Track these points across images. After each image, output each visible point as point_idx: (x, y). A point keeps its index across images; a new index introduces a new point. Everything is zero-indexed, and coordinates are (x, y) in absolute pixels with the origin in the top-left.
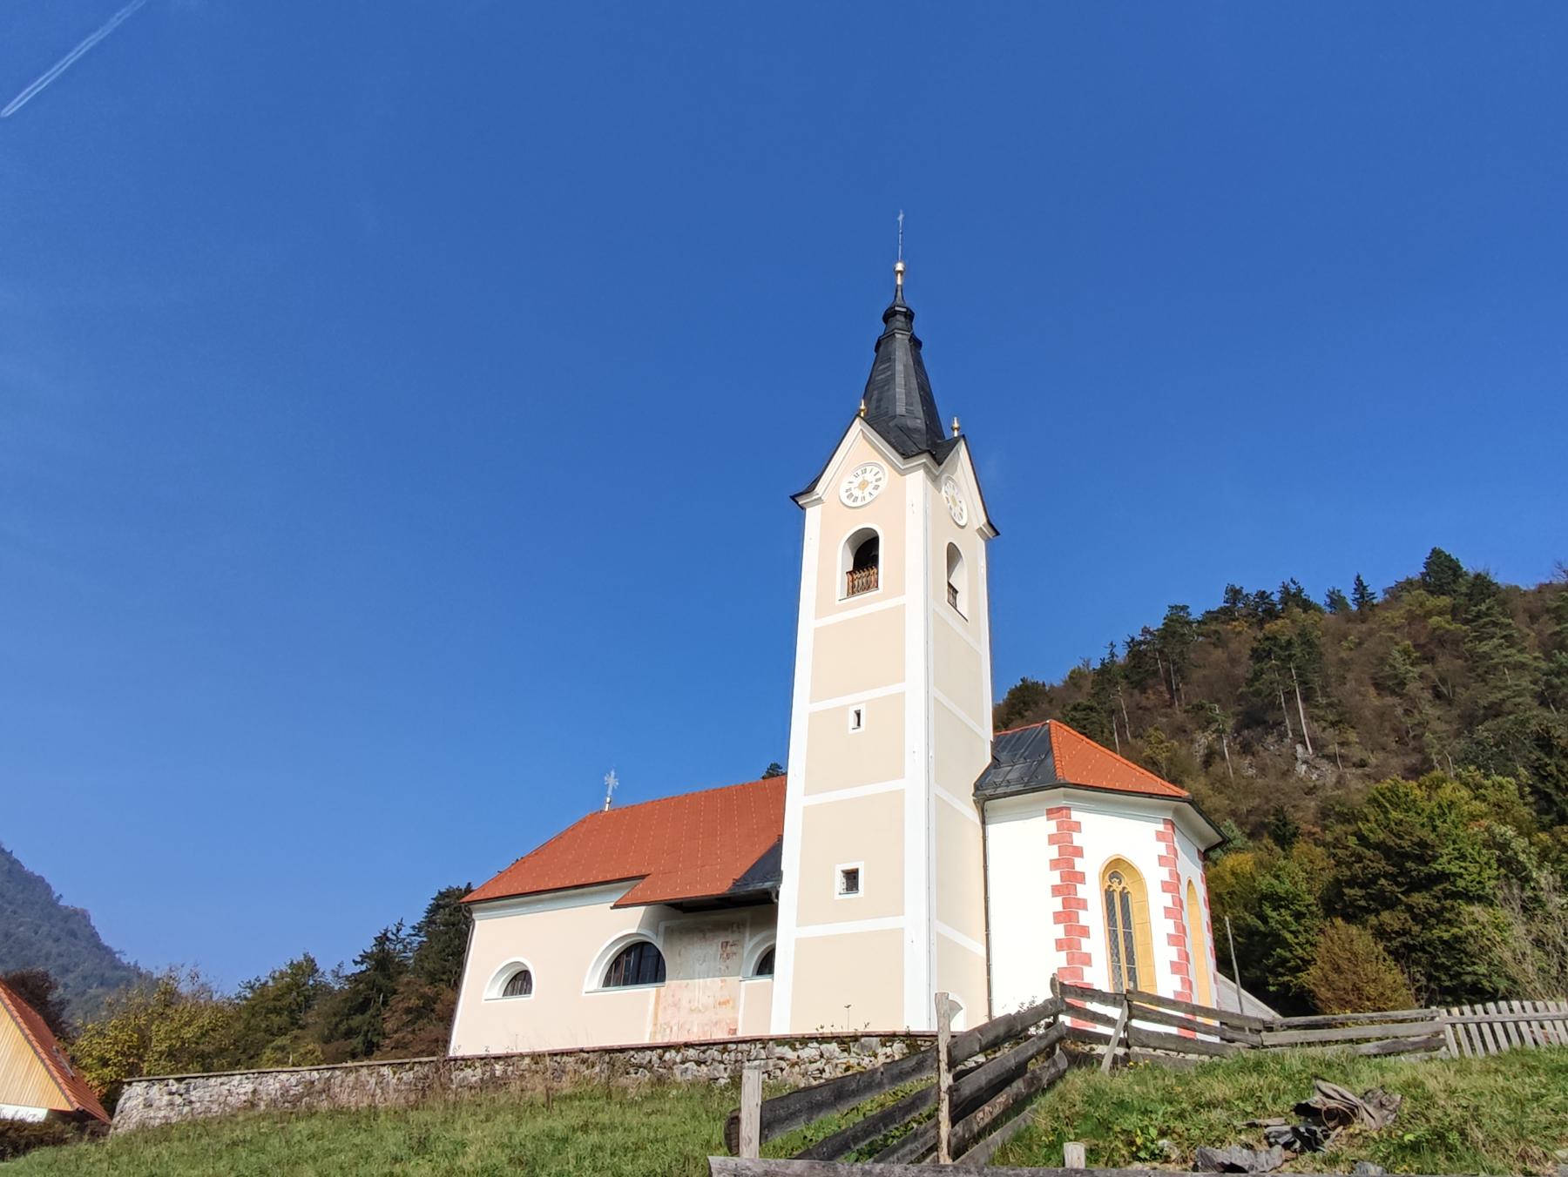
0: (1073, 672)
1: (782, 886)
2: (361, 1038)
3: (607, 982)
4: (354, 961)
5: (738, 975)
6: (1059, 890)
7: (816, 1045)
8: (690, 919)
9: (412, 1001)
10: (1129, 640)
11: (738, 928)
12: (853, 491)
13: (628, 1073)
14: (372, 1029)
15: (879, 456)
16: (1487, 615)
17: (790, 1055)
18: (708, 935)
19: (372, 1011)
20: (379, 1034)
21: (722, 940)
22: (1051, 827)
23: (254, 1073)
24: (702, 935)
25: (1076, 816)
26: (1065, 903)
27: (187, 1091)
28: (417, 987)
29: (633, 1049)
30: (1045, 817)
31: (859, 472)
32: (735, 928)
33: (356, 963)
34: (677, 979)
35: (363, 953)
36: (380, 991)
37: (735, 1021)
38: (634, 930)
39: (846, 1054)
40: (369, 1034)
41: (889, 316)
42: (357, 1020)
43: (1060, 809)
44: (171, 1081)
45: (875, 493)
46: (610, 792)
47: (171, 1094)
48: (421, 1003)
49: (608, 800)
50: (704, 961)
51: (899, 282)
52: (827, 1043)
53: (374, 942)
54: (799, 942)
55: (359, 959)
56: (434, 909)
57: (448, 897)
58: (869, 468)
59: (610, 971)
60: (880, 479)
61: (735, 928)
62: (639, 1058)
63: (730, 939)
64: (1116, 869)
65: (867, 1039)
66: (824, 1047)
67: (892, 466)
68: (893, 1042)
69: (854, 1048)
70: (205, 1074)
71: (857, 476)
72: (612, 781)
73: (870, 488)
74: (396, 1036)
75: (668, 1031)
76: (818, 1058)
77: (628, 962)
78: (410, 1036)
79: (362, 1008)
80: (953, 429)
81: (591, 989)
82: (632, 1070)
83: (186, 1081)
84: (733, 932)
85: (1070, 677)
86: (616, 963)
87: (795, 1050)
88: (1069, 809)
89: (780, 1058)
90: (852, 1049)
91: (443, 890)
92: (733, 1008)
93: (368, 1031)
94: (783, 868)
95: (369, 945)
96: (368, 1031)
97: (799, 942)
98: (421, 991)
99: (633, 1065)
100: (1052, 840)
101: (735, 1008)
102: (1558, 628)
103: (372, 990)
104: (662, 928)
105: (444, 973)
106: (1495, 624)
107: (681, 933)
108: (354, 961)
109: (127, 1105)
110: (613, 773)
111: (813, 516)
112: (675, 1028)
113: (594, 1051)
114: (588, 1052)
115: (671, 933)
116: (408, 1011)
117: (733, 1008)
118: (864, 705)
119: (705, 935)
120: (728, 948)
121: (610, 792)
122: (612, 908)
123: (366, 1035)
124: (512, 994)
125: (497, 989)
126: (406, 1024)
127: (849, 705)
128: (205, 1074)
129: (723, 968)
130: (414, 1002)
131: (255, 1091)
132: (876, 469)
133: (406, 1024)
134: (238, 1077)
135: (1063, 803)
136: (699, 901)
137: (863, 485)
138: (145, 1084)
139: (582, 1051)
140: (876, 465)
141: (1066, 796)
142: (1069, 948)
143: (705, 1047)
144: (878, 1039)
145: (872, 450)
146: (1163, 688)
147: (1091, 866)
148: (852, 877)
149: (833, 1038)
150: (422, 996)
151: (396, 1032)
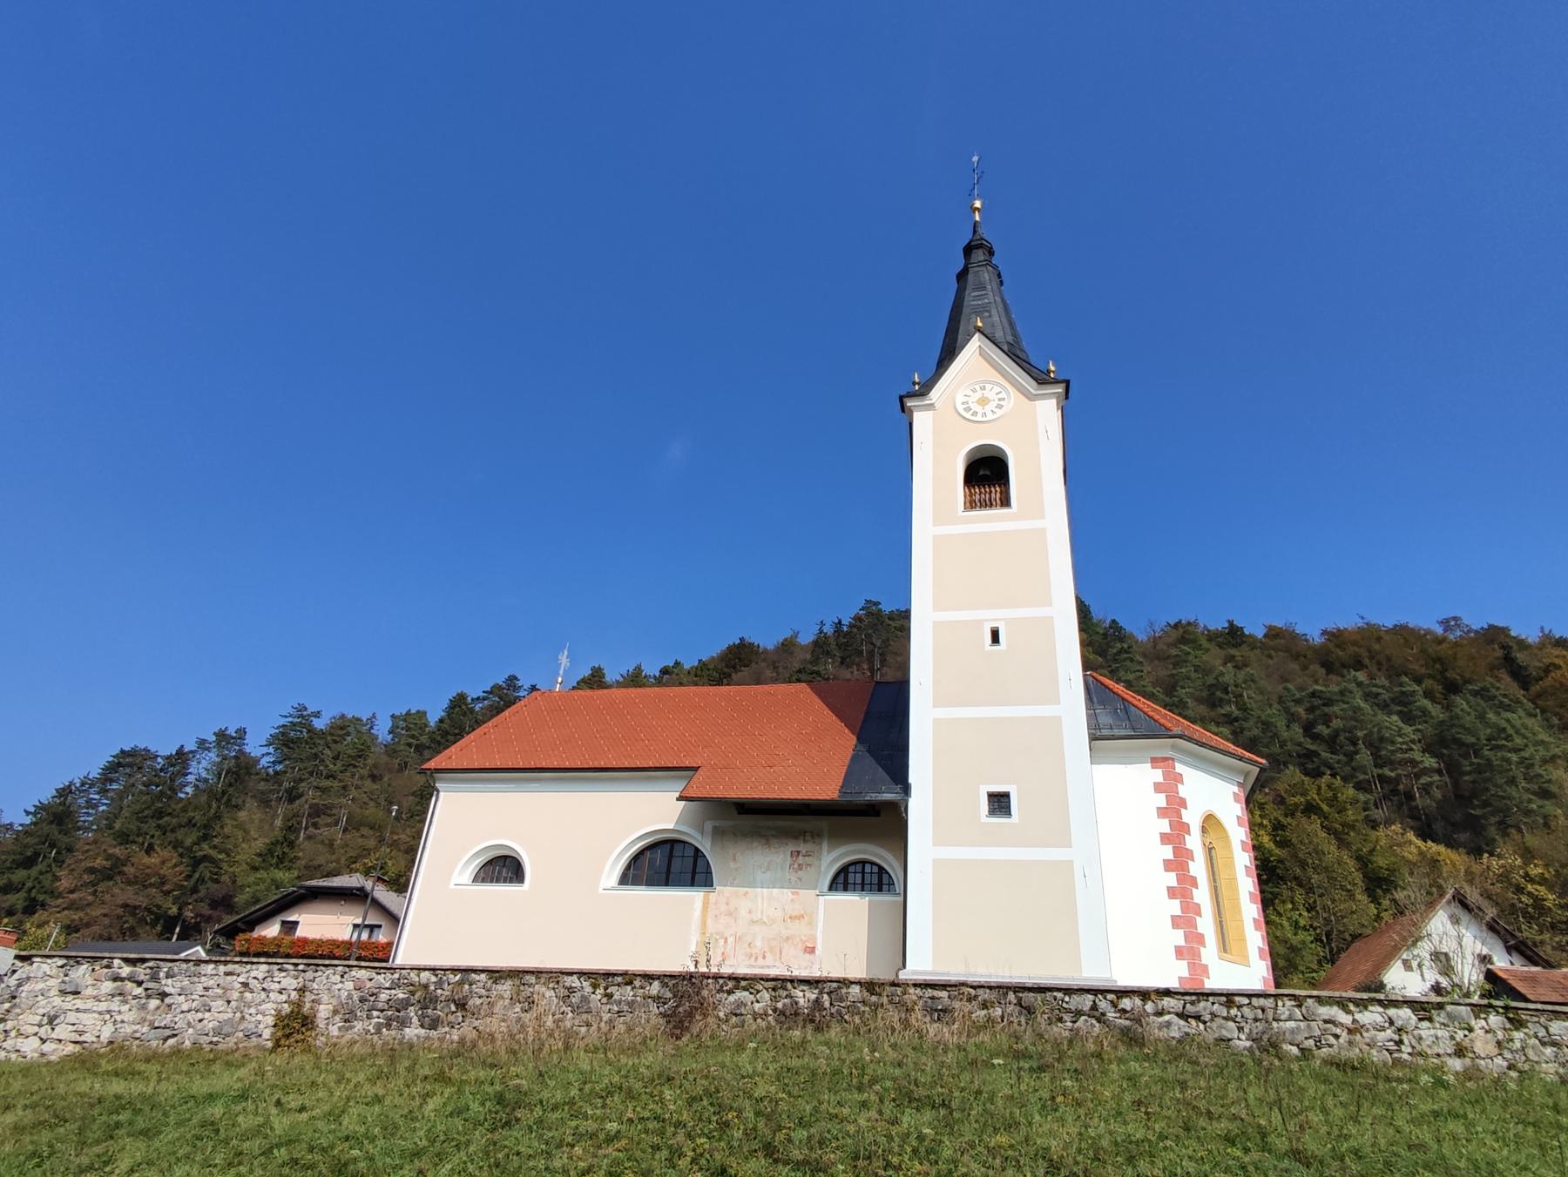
0: (786, 640)
1: (910, 800)
2: (22, 894)
3: (625, 879)
4: (25, 811)
5: (815, 889)
6: (1168, 839)
7: (1380, 1009)
8: (748, 821)
9: (98, 861)
10: (837, 621)
11: (812, 837)
12: (970, 404)
13: (1060, 1020)
14: (38, 886)
15: (999, 376)
16: (1126, 652)
17: (1345, 1019)
18: (774, 841)
19: (40, 867)
20: (45, 893)
21: (791, 847)
22: (1158, 775)
23: (296, 965)
24: (764, 842)
25: (1180, 768)
26: (1176, 851)
27: (155, 978)
28: (104, 847)
29: (1059, 990)
30: (1149, 765)
31: (977, 387)
32: (808, 838)
33: (28, 813)
34: (732, 885)
35: (38, 804)
36: (52, 846)
37: (814, 939)
38: (671, 826)
39: (1425, 1024)
40: (34, 891)
41: (968, 250)
42: (20, 875)
43: (1166, 759)
44: (116, 962)
45: (999, 413)
46: (561, 672)
47: (116, 979)
48: (107, 864)
49: (560, 680)
50: (768, 869)
51: (977, 218)
52: (1396, 1007)
53: (55, 793)
54: (938, 864)
55: (32, 810)
56: (113, 768)
57: (132, 756)
58: (988, 386)
59: (628, 867)
60: (1004, 399)
61: (808, 838)
62: (1075, 1002)
63: (803, 848)
64: (1210, 823)
65: (1453, 1007)
66: (1392, 1012)
67: (1019, 390)
68: (1488, 1013)
69: (1440, 1017)
70: (223, 959)
71: (974, 391)
72: (564, 660)
73: (992, 406)
74: (71, 896)
75: (722, 942)
76: (1387, 1025)
77: (652, 862)
78: (90, 898)
79: (29, 862)
80: (914, 383)
81: (609, 886)
82: (1067, 1017)
83: (151, 964)
84: (805, 841)
85: (783, 644)
86: (637, 858)
87: (1348, 1012)
88: (1173, 759)
89: (1326, 1022)
90: (1437, 1018)
91: (127, 749)
92: (810, 924)
93: (34, 887)
94: (910, 781)
95: (47, 794)
96: (34, 887)
97: (938, 864)
98: (110, 852)
99: (1069, 1011)
100: (1158, 788)
101: (812, 924)
102: (1174, 672)
103: (44, 843)
104: (709, 825)
105: (138, 836)
106: (1132, 660)
107: (735, 835)
108: (25, 811)
109: (26, 988)
110: (566, 653)
111: (923, 422)
112: (731, 940)
113: (990, 988)
114: (972, 987)
115: (719, 834)
116: (91, 871)
117: (810, 924)
118: (1003, 623)
119: (767, 840)
120: (800, 857)
121: (561, 672)
122: (677, 799)
123: (30, 890)
124: (483, 881)
125: (464, 874)
126: (85, 885)
127: (986, 620)
128: (223, 959)
129: (793, 879)
130: (99, 862)
131: (302, 990)
132: (997, 389)
133: (85, 885)
134: (264, 968)
135: (1169, 754)
136: (772, 804)
137: (983, 401)
138: (61, 962)
139: (964, 984)
140: (998, 384)
141: (1173, 747)
142: (1183, 896)
143: (1194, 998)
144: (1469, 1008)
145: (989, 367)
146: (865, 666)
147: (1192, 817)
148: (999, 803)
149: (1405, 1002)
150: (109, 857)
151: (72, 892)
